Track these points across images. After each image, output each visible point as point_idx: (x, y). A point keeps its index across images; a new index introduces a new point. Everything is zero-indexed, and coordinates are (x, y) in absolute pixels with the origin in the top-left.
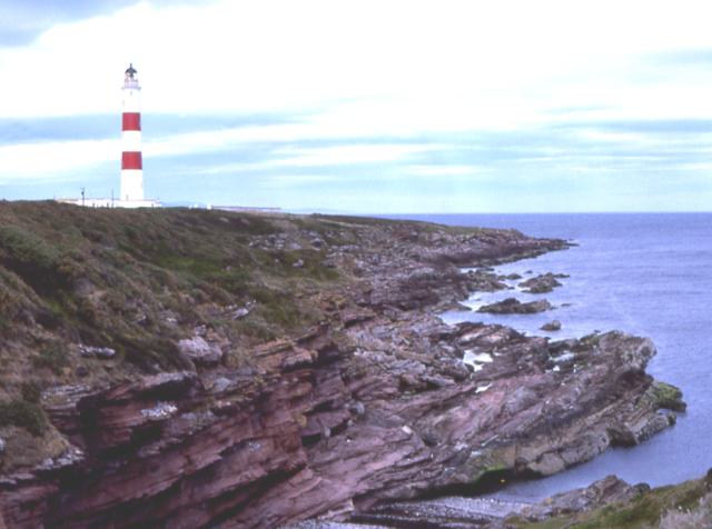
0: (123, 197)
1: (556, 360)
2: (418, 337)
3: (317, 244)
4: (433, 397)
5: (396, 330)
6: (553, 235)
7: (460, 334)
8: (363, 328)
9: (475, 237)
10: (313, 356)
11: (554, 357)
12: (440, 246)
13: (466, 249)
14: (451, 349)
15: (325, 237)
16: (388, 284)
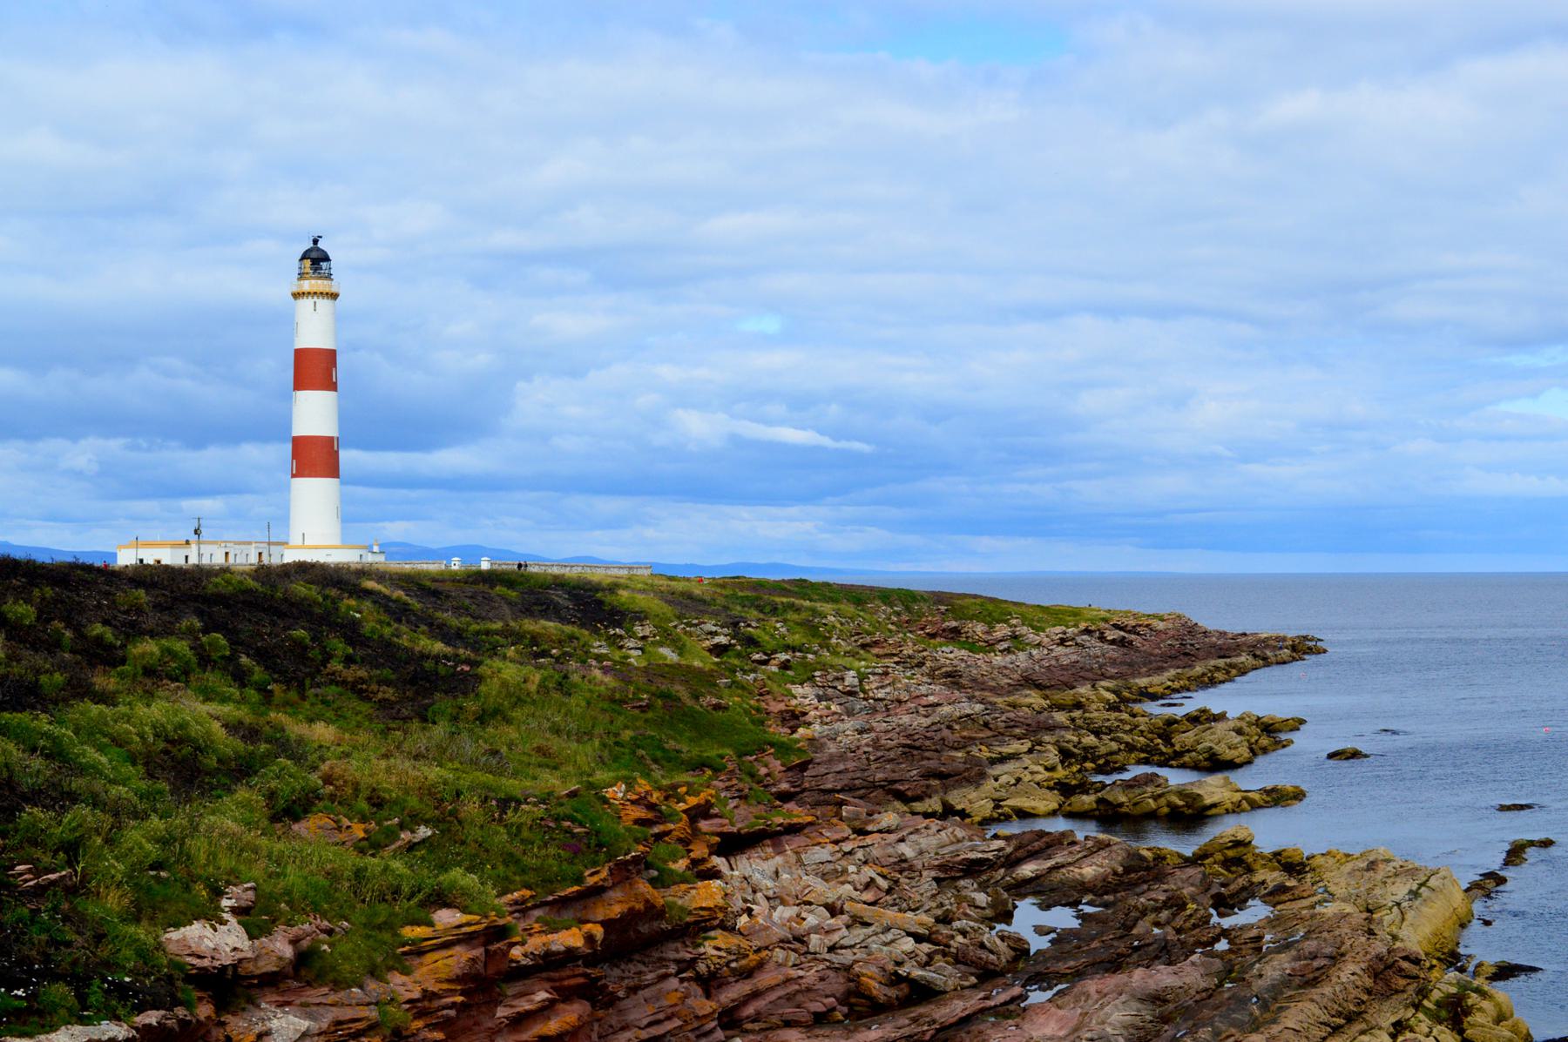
0: (295, 539)
1: (1227, 922)
2: (911, 868)
3: (719, 650)
4: (915, 1020)
5: (860, 855)
6: (1290, 627)
7: (1012, 862)
8: (781, 852)
9: (1087, 631)
10: (590, 938)
11: (1221, 915)
12: (1008, 650)
13: (1066, 655)
14: (982, 898)
16: (876, 741)
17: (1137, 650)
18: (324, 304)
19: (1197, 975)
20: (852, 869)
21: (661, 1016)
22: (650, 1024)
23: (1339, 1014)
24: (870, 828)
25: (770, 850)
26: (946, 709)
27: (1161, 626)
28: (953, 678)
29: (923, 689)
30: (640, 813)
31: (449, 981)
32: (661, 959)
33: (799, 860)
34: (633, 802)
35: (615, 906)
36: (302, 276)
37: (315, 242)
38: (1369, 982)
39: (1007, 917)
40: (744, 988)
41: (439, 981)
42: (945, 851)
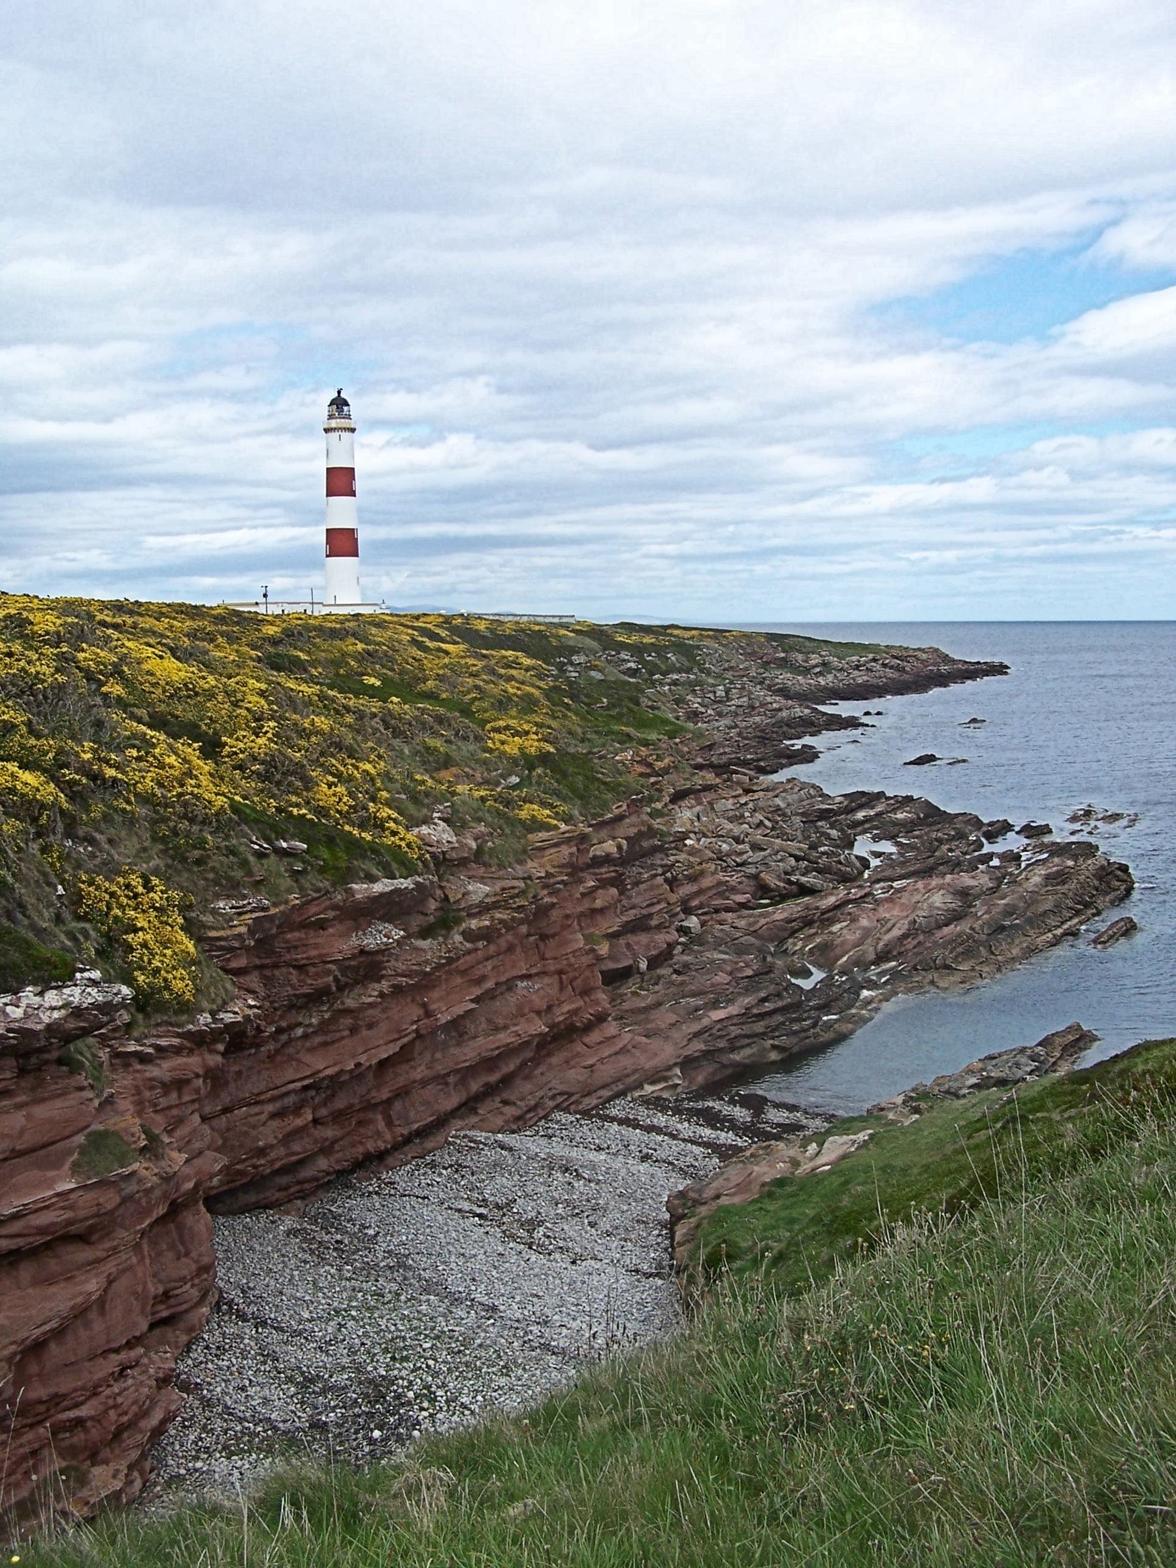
5: (751, 805)
10: (619, 847)
12: (820, 674)
14: (834, 833)
15: (641, 661)
16: (739, 734)
17: (907, 673)
18: (346, 435)
19: (987, 879)
20: (747, 814)
21: (655, 900)
22: (648, 906)
23: (1079, 903)
24: (755, 788)
25: (693, 802)
26: (785, 714)
27: (924, 656)
28: (784, 692)
29: (769, 699)
30: (641, 769)
31: (559, 867)
32: (653, 865)
33: (713, 809)
34: (638, 762)
35: (629, 828)
36: (331, 417)
37: (339, 392)
38: (1096, 883)
39: (851, 845)
40: (694, 888)
41: (554, 867)
42: (804, 803)
